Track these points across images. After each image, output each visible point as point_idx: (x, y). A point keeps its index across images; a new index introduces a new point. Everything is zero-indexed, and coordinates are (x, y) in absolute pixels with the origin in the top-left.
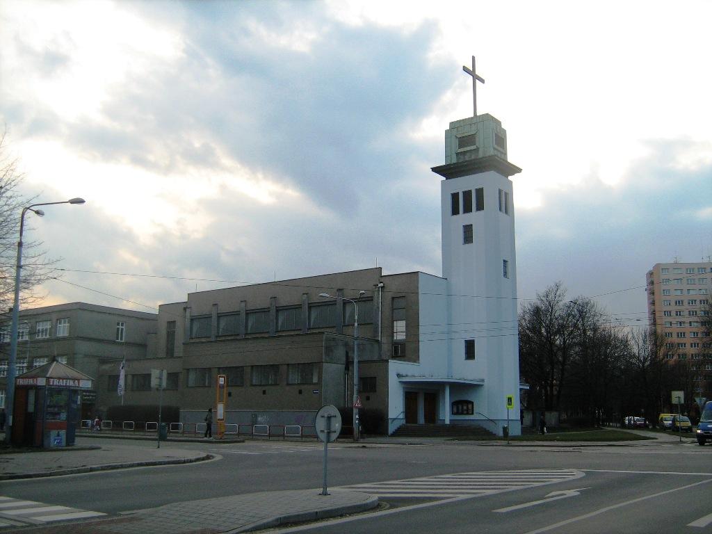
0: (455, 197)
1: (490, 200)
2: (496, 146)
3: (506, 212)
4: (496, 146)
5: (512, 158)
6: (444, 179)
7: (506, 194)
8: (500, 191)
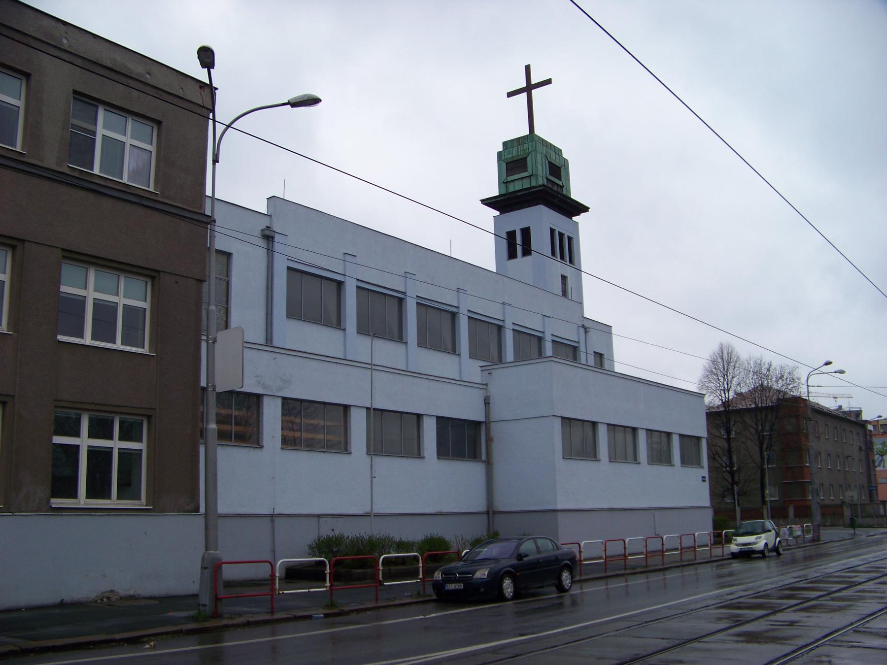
0: (511, 235)
1: (541, 241)
2: (551, 178)
3: (571, 261)
4: (551, 178)
5: (577, 193)
6: (497, 213)
7: (570, 239)
8: (552, 231)
